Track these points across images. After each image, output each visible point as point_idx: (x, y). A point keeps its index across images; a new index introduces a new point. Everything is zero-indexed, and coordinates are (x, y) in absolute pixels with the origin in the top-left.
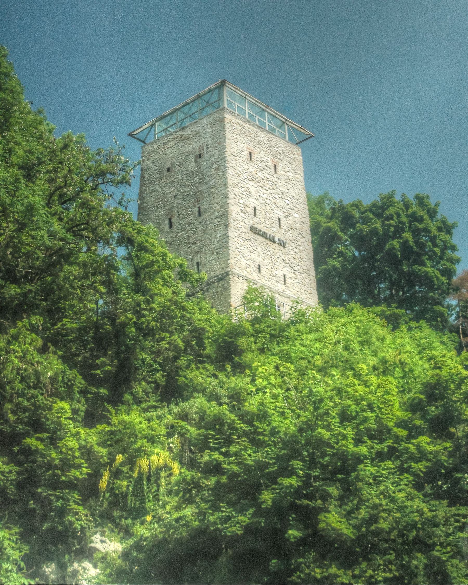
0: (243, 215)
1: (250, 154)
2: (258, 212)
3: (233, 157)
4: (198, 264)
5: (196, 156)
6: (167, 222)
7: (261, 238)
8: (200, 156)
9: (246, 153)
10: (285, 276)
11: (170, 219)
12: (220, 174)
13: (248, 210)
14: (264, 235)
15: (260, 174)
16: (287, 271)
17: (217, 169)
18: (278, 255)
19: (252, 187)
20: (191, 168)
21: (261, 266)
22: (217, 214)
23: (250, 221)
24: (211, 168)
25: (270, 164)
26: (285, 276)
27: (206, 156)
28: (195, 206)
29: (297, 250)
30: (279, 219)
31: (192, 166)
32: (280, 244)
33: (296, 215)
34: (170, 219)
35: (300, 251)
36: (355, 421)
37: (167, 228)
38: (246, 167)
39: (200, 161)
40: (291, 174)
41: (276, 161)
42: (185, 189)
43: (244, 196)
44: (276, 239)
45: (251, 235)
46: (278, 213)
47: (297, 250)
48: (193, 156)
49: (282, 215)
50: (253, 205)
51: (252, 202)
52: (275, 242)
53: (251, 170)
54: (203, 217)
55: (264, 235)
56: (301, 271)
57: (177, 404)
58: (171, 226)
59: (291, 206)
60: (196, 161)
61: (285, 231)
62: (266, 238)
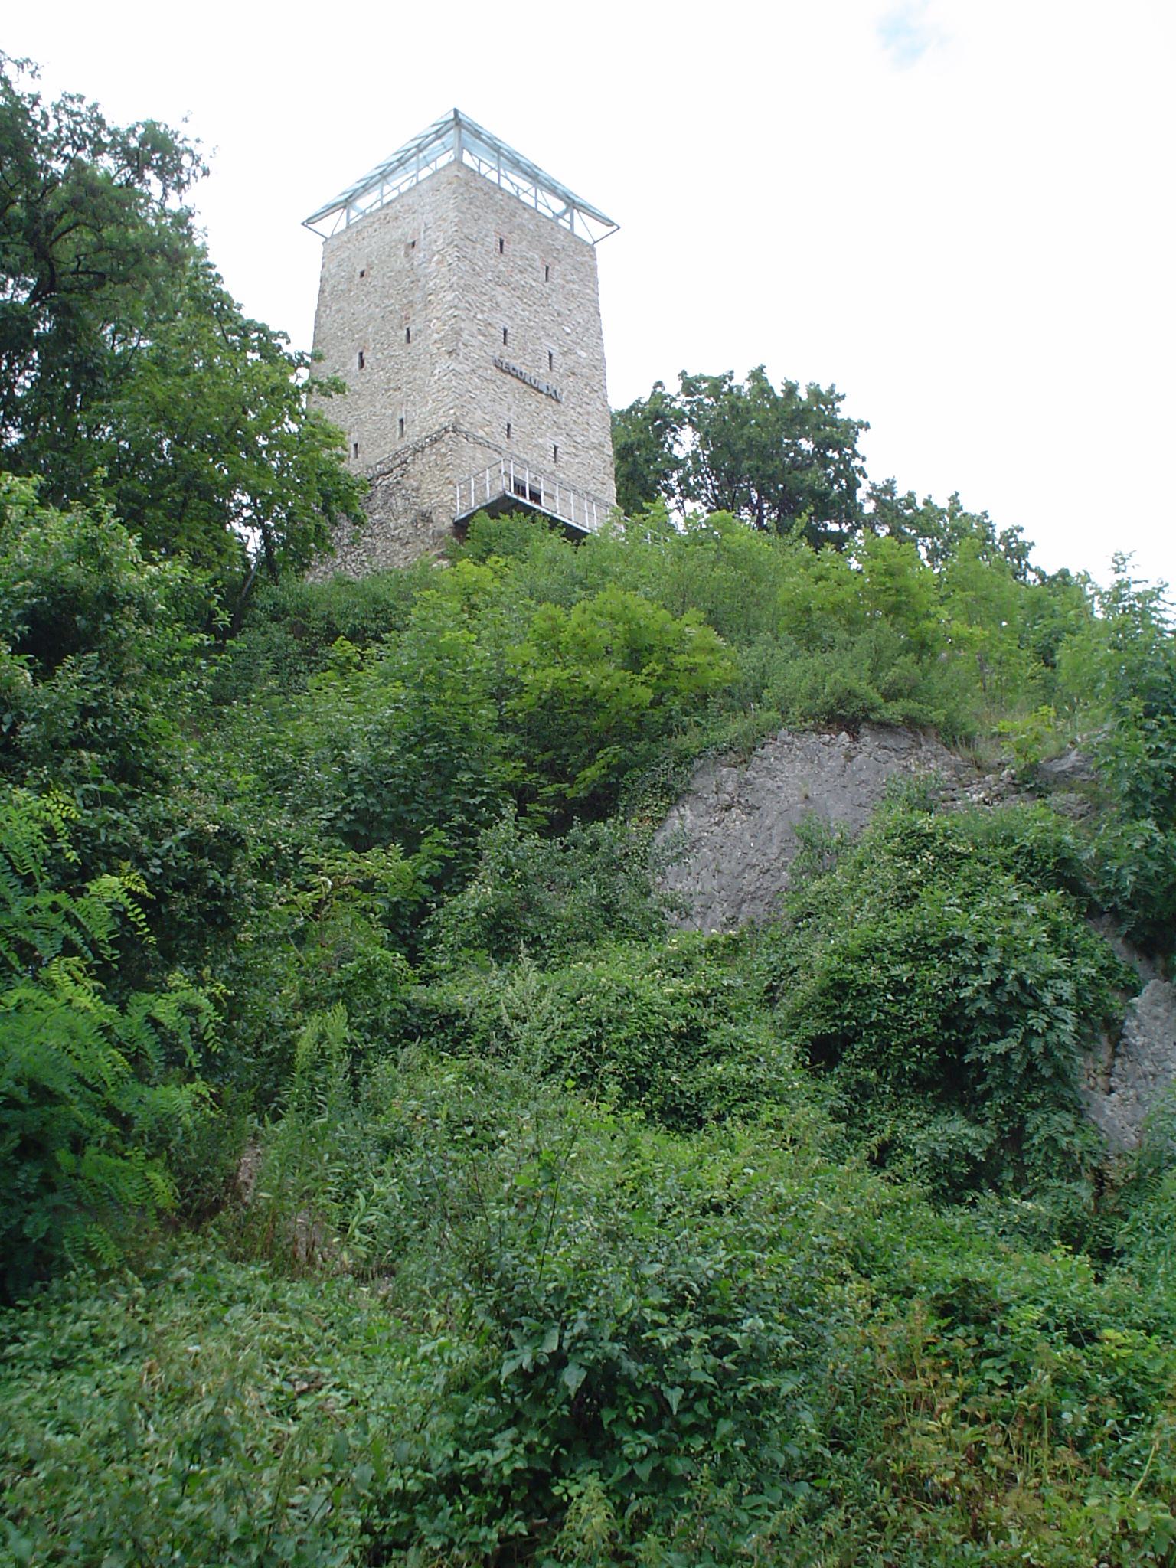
0: (481, 338)
2: (510, 338)
3: (467, 242)
4: (401, 421)
5: (407, 247)
6: (357, 359)
7: (515, 382)
8: (413, 244)
9: (493, 242)
10: (556, 448)
11: (361, 354)
12: (444, 270)
13: (493, 331)
14: (519, 376)
15: (518, 277)
16: (561, 440)
17: (439, 262)
18: (545, 413)
19: (501, 295)
20: (398, 266)
22: (436, 336)
23: (496, 350)
24: (430, 261)
25: (538, 263)
26: (556, 448)
27: (421, 244)
28: (401, 328)
29: (581, 411)
30: (551, 356)
31: (400, 262)
32: (549, 396)
33: (584, 355)
34: (361, 354)
35: (588, 413)
36: (646, 1437)
37: (357, 366)
38: (492, 262)
39: (413, 252)
40: (576, 286)
41: (550, 260)
42: (386, 301)
44: (542, 387)
45: (492, 372)
47: (578, 409)
48: (402, 246)
49: (556, 351)
50: (502, 325)
51: (501, 321)
53: (501, 267)
54: (415, 343)
55: (519, 376)
56: (587, 444)
57: (816, 850)
58: (362, 364)
59: (573, 336)
60: (407, 255)
61: (561, 376)
62: (524, 382)
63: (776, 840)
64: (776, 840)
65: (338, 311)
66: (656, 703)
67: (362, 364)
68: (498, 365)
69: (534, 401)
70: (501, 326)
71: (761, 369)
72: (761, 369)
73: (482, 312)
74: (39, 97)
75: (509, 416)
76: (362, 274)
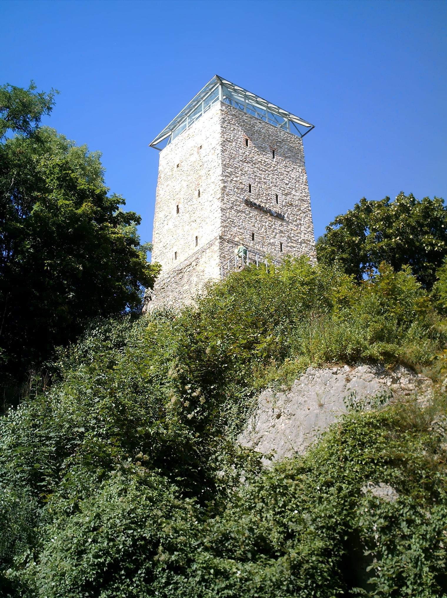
10: (281, 244)
11: (178, 206)
23: (245, 195)
26: (281, 244)
34: (178, 206)
45: (243, 206)
46: (275, 190)
58: (178, 211)
60: (198, 153)
63: (301, 434)
64: (301, 434)
65: (167, 186)
66: (424, 449)
67: (178, 211)
68: (249, 203)
69: (267, 220)
70: (247, 183)
71: (125, 204)
72: (125, 204)
73: (237, 177)
74: (36, 87)
76: (178, 166)
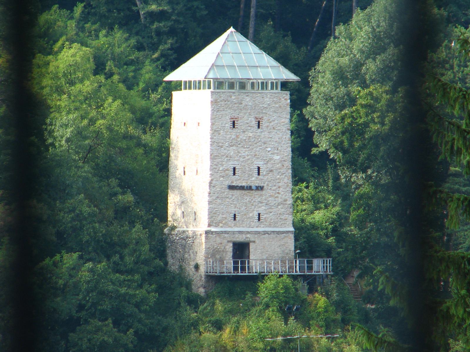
1: (234, 122)
14: (242, 188)
21: (237, 214)
43: (224, 163)
45: (232, 192)
52: (253, 190)
75: (233, 210)
